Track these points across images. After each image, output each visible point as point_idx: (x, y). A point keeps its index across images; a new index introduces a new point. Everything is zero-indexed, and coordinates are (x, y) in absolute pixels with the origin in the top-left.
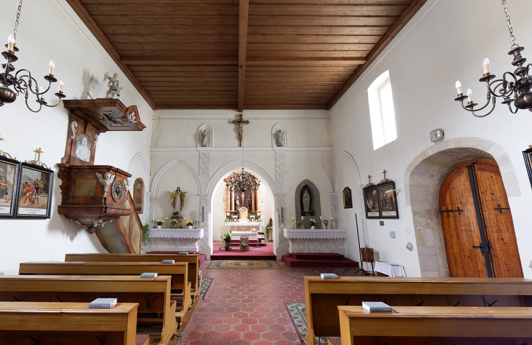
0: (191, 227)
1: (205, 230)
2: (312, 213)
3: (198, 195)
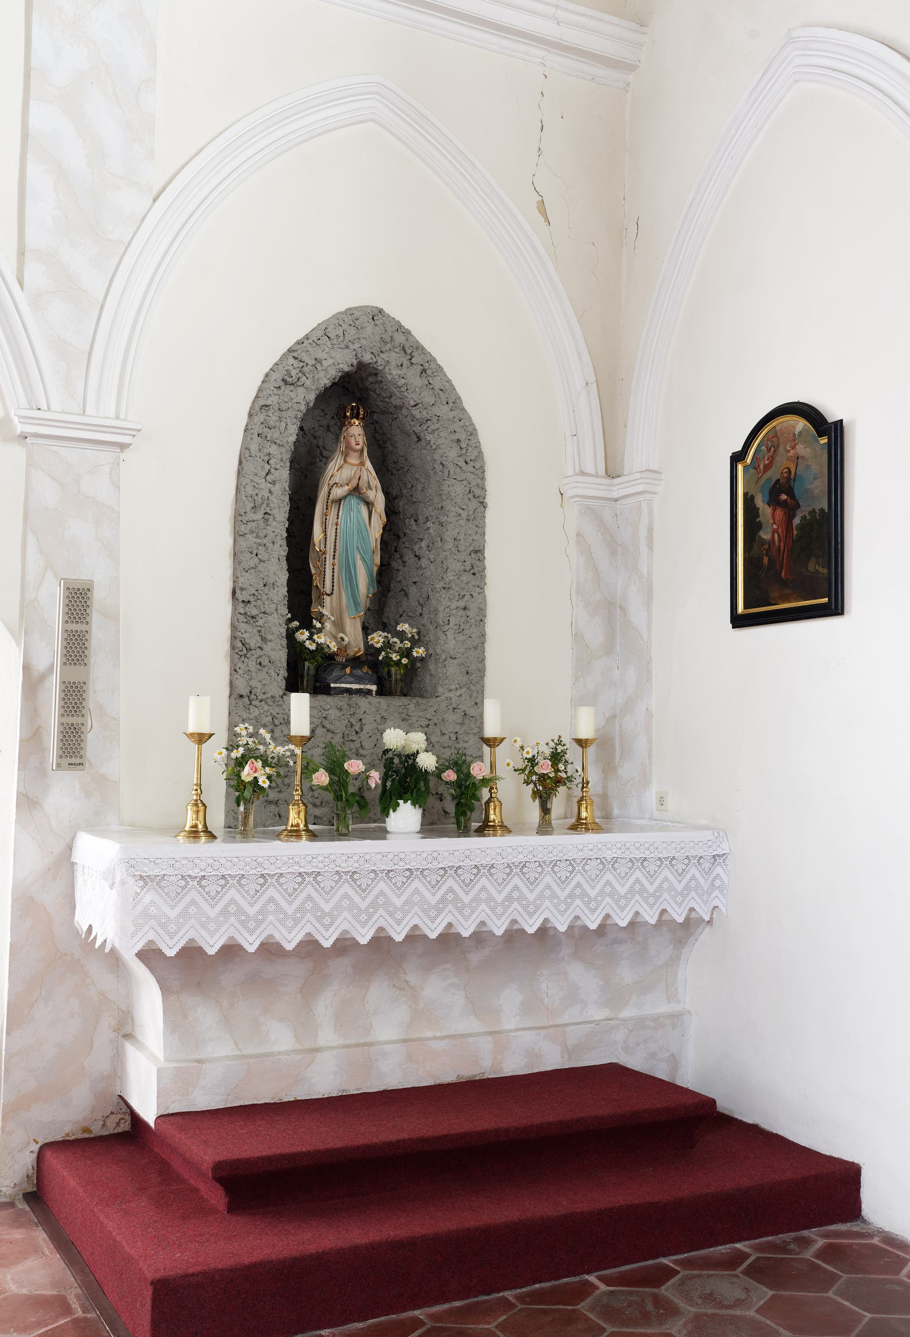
2: (395, 678)
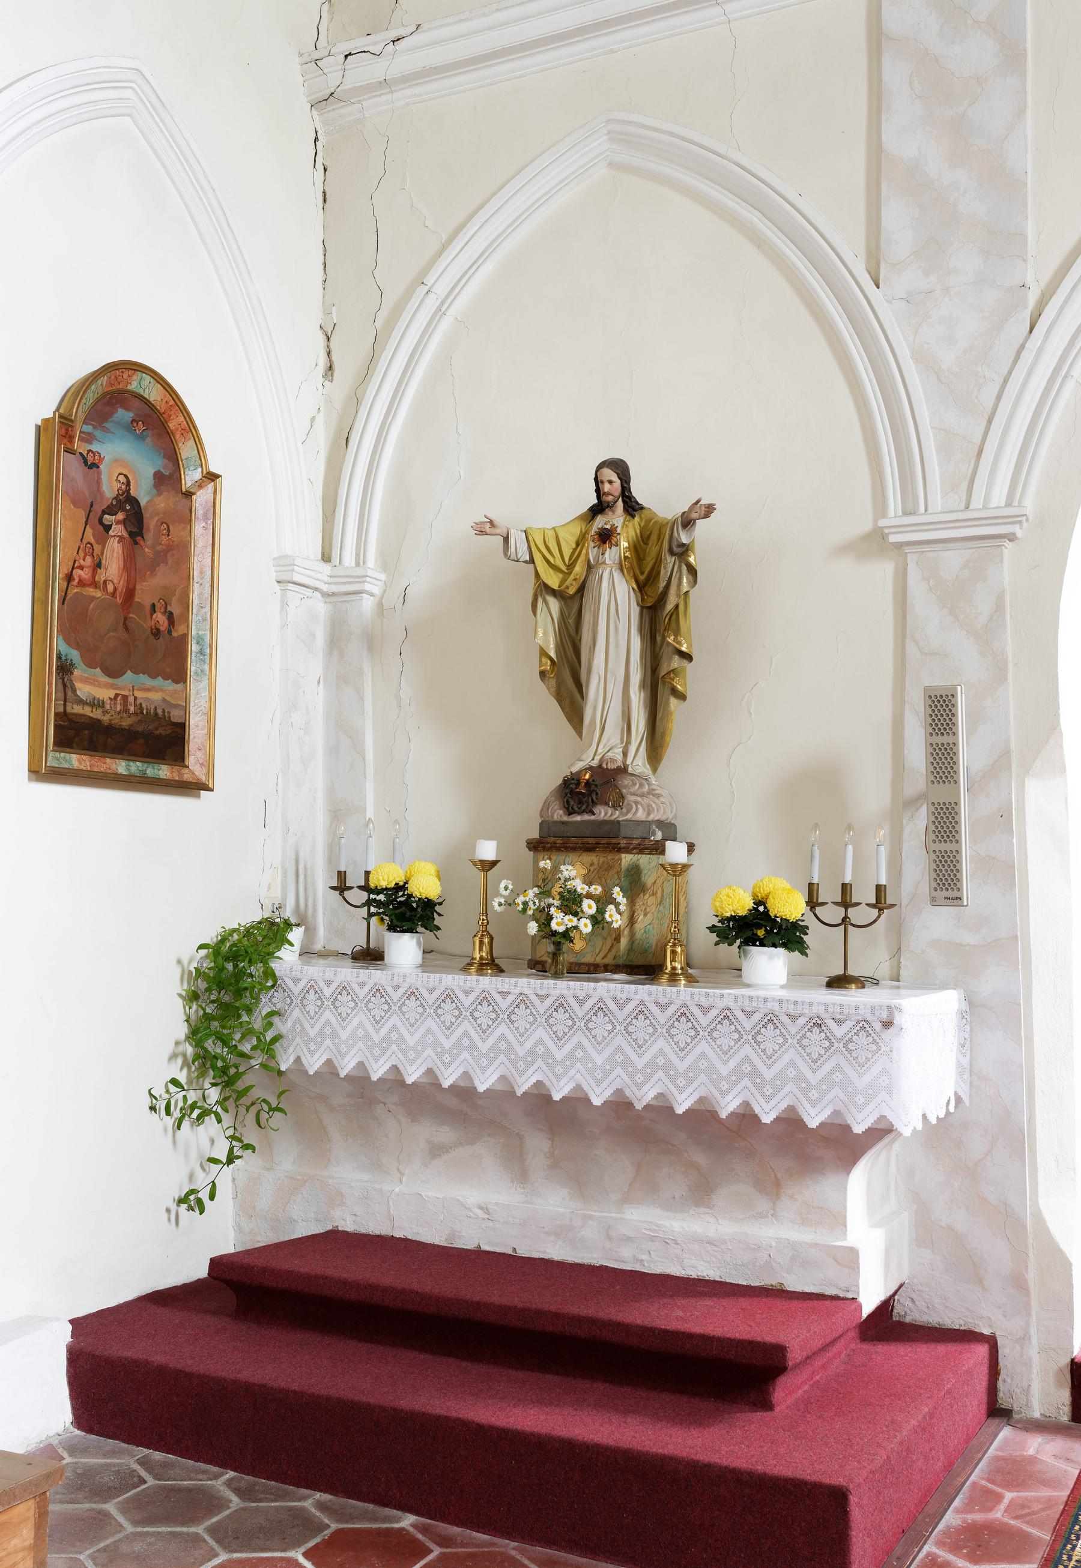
0: (769, 966)
1: (974, 1011)
3: (875, 543)
